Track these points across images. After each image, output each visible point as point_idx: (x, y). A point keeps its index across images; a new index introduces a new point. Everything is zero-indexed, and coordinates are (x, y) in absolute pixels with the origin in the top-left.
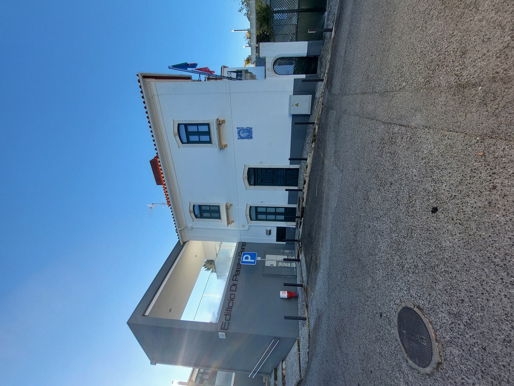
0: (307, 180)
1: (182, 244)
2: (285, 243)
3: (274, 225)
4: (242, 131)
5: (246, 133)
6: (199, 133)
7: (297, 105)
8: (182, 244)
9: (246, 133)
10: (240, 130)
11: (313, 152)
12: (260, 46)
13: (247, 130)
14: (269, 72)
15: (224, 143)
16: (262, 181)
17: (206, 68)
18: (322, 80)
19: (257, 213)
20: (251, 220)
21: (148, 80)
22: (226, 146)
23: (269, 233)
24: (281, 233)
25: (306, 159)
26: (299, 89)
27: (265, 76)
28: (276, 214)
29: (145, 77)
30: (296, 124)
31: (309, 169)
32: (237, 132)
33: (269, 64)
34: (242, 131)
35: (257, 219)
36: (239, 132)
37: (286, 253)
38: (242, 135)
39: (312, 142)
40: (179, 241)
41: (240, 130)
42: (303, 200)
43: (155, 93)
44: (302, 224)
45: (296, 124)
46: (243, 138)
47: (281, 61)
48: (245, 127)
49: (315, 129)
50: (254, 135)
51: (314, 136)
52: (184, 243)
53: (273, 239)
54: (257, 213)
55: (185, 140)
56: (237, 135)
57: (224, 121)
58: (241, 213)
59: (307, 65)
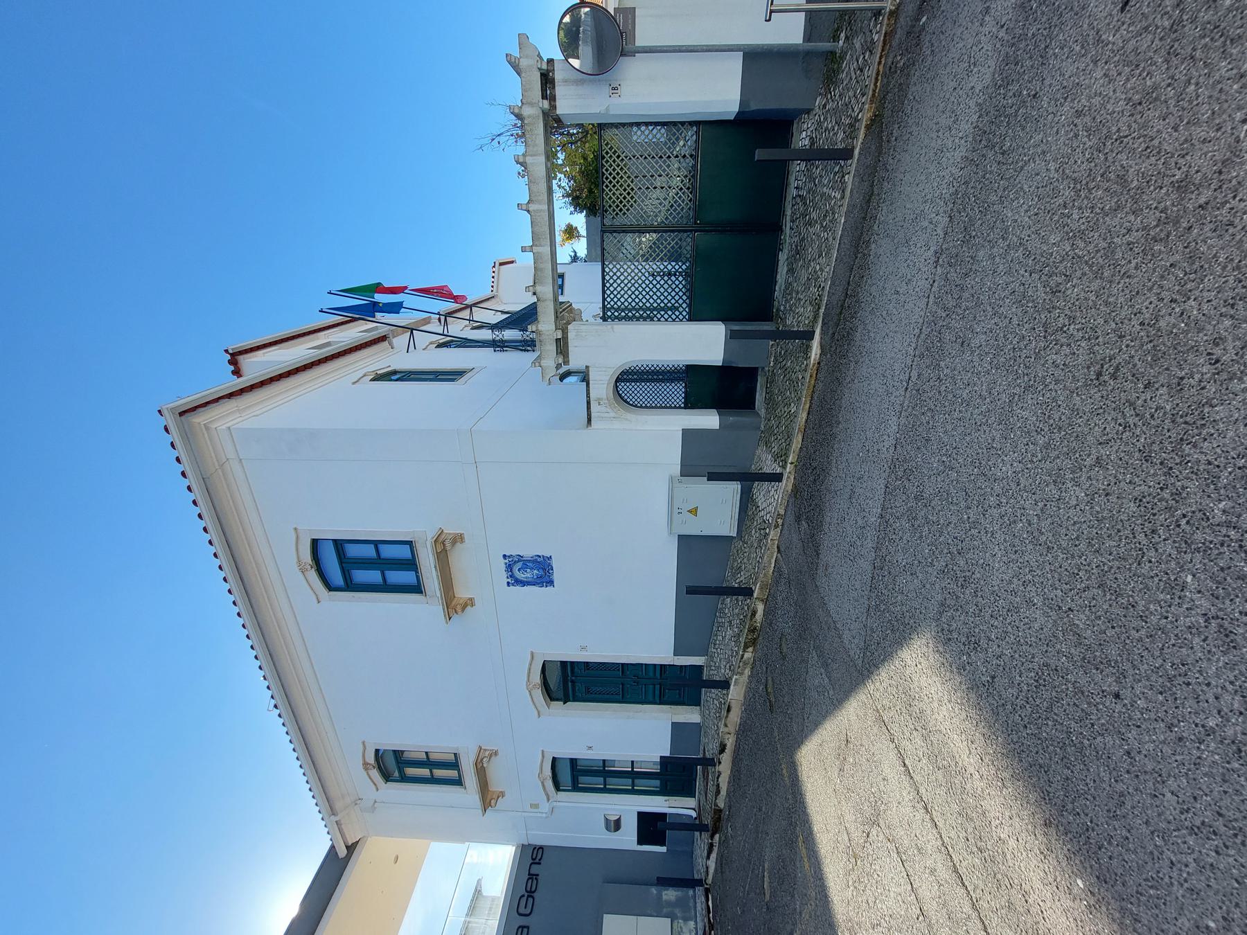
0: (730, 742)
1: (342, 852)
2: (663, 849)
3: (629, 807)
4: (519, 565)
5: (534, 571)
6: (380, 563)
7: (694, 511)
8: (342, 852)
9: (534, 571)
10: (513, 563)
11: (747, 672)
12: (571, 335)
13: (535, 561)
14: (602, 408)
15: (462, 593)
16: (588, 691)
17: (442, 288)
18: (777, 478)
19: (574, 775)
20: (557, 786)
21: (200, 419)
22: (470, 602)
23: (617, 825)
24: (651, 827)
25: (725, 685)
26: (700, 460)
27: (589, 420)
28: (633, 775)
29: (182, 414)
30: (692, 591)
31: (735, 717)
32: (503, 567)
33: (602, 386)
34: (519, 565)
35: (576, 788)
36: (509, 568)
37: (669, 904)
38: (520, 575)
39: (746, 647)
40: (333, 847)
41: (513, 563)
42: (718, 792)
43: (231, 455)
44: (716, 849)
45: (692, 591)
46: (523, 583)
47: (636, 383)
48: (528, 553)
49: (754, 613)
50: (556, 577)
51: (752, 630)
52: (351, 848)
53: (628, 838)
54: (574, 775)
55: (338, 579)
56: (504, 575)
57: (458, 539)
58: (523, 776)
59: (719, 387)
